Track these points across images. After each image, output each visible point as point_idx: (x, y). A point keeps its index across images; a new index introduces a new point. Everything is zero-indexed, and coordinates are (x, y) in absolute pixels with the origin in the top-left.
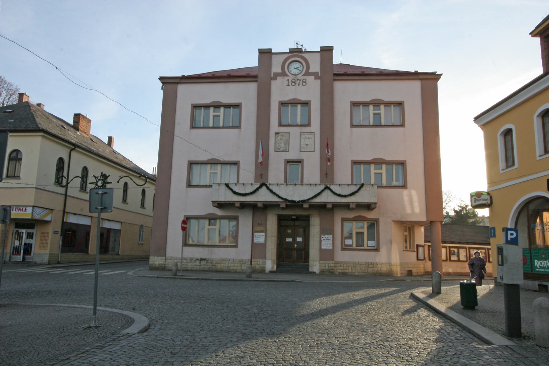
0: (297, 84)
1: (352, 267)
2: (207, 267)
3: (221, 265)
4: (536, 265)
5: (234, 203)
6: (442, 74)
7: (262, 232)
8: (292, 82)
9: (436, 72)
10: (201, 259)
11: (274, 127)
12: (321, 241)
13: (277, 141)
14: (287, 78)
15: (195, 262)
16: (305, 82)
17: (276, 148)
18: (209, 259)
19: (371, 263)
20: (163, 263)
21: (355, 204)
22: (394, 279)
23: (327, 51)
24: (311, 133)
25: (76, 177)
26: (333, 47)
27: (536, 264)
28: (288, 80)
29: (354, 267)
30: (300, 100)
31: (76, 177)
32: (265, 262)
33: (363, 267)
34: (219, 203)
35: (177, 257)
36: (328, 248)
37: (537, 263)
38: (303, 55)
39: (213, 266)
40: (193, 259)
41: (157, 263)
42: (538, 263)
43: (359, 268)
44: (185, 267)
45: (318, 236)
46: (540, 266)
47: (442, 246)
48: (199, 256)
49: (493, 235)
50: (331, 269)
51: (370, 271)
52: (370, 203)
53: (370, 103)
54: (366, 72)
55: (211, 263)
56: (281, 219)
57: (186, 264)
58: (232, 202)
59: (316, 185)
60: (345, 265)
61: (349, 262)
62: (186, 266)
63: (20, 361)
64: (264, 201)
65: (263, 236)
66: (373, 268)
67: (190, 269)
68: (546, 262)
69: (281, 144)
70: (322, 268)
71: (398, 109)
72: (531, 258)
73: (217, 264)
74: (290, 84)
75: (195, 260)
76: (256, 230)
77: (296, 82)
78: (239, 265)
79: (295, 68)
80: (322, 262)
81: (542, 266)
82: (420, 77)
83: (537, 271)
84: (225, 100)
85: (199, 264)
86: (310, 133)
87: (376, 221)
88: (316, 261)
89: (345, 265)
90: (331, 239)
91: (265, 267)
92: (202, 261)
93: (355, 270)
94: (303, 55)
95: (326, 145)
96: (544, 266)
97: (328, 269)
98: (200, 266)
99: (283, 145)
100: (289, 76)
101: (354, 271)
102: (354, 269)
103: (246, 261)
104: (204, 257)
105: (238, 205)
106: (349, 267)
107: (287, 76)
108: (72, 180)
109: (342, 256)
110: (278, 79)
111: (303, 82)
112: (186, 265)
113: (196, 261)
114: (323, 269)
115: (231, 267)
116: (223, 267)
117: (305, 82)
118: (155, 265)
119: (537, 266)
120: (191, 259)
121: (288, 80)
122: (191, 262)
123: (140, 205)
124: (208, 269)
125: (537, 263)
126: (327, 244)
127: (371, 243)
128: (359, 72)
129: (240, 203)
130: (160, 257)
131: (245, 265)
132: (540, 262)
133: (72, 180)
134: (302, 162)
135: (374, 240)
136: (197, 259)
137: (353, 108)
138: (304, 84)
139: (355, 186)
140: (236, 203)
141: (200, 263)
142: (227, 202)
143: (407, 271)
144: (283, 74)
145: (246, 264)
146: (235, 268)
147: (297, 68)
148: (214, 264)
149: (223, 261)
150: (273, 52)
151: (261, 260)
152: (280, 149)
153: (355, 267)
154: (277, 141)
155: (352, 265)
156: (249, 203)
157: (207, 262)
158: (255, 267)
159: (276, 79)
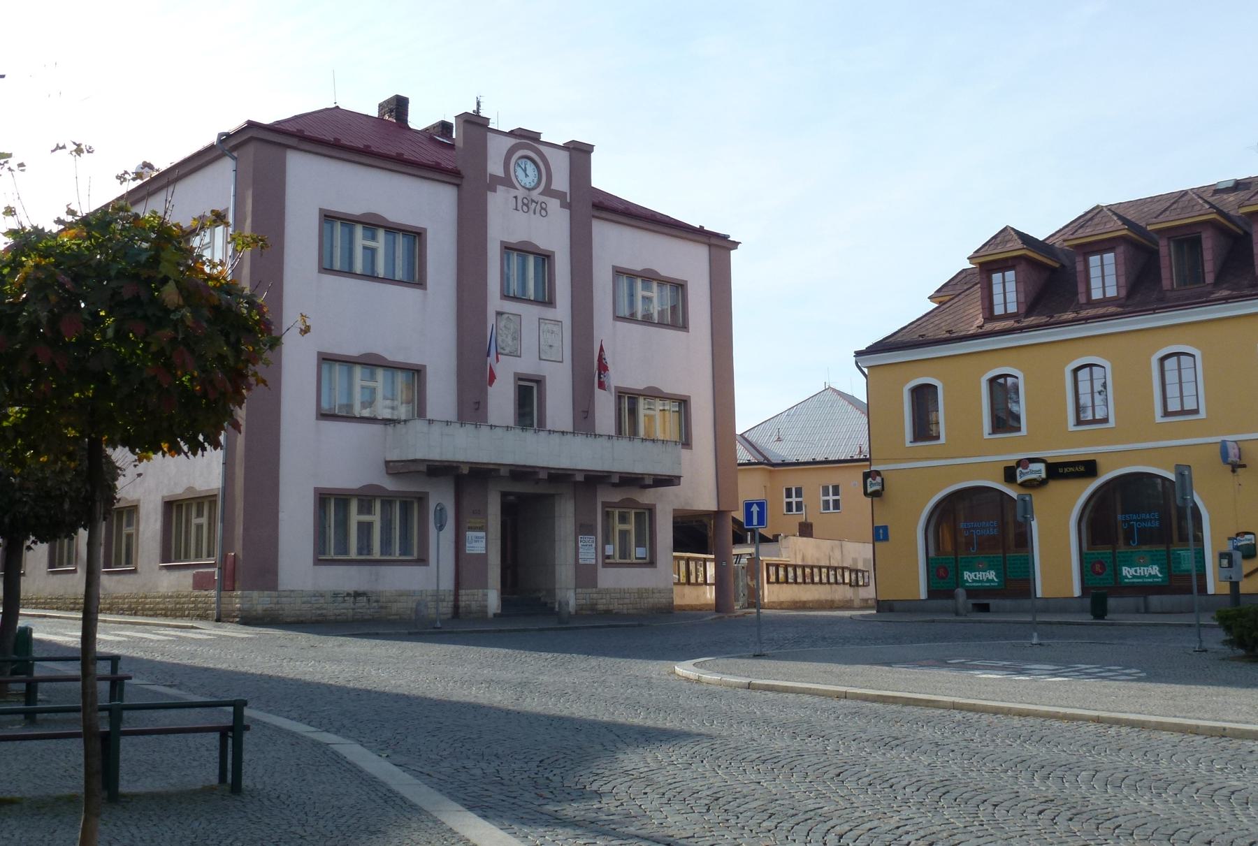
0: (531, 212)
2: (368, 611)
3: (399, 604)
4: (965, 579)
5: (459, 464)
7: (480, 529)
8: (524, 204)
9: (729, 236)
10: (357, 595)
11: (495, 302)
12: (577, 548)
13: (501, 332)
14: (513, 192)
15: (344, 601)
17: (498, 347)
18: (372, 592)
19: (646, 589)
21: (652, 477)
23: (580, 153)
24: (556, 323)
26: (592, 146)
27: (1124, 572)
28: (516, 197)
30: (537, 247)
32: (486, 595)
34: (430, 463)
35: (302, 591)
36: (588, 562)
37: (1126, 571)
38: (542, 148)
39: (381, 607)
40: (339, 594)
41: (260, 608)
42: (969, 576)
44: (322, 614)
45: (572, 538)
46: (973, 580)
47: (674, 556)
48: (351, 586)
49: (881, 537)
52: (673, 476)
53: (639, 274)
54: (607, 203)
55: (377, 601)
56: (335, 499)
58: (455, 464)
59: (563, 433)
60: (608, 596)
61: (615, 589)
62: (324, 611)
63: (520, 798)
64: (472, 463)
65: (482, 538)
67: (333, 618)
68: (984, 573)
69: (507, 337)
72: (957, 567)
73: (390, 604)
74: (519, 208)
75: (344, 597)
76: (469, 525)
77: (529, 205)
79: (527, 175)
80: (579, 590)
81: (977, 579)
82: (714, 241)
83: (1127, 583)
84: (395, 215)
85: (352, 606)
86: (555, 321)
88: (570, 589)
89: (608, 596)
90: (594, 545)
91: (486, 607)
92: (358, 599)
93: (623, 604)
94: (542, 148)
96: (1142, 574)
98: (353, 609)
99: (509, 340)
100: (517, 189)
103: (445, 596)
104: (362, 588)
105: (616, 480)
107: (515, 188)
109: (610, 579)
110: (498, 189)
111: (542, 208)
112: (325, 609)
113: (346, 598)
114: (583, 605)
117: (545, 209)
118: (254, 613)
119: (1126, 576)
120: (336, 595)
121: (516, 197)
122: (334, 602)
124: (371, 617)
125: (1126, 571)
126: (588, 554)
127: (641, 552)
128: (621, 207)
129: (585, 473)
130: (266, 592)
131: (444, 603)
132: (1133, 569)
135: (645, 547)
136: (349, 595)
138: (543, 213)
139: (652, 442)
140: (462, 466)
141: (354, 603)
142: (446, 464)
144: (507, 182)
145: (445, 601)
147: (525, 171)
148: (384, 605)
149: (402, 596)
150: (543, 139)
151: (481, 591)
152: (504, 350)
154: (501, 332)
155: (618, 595)
156: (485, 466)
157: (369, 600)
158: (470, 606)
159: (495, 191)
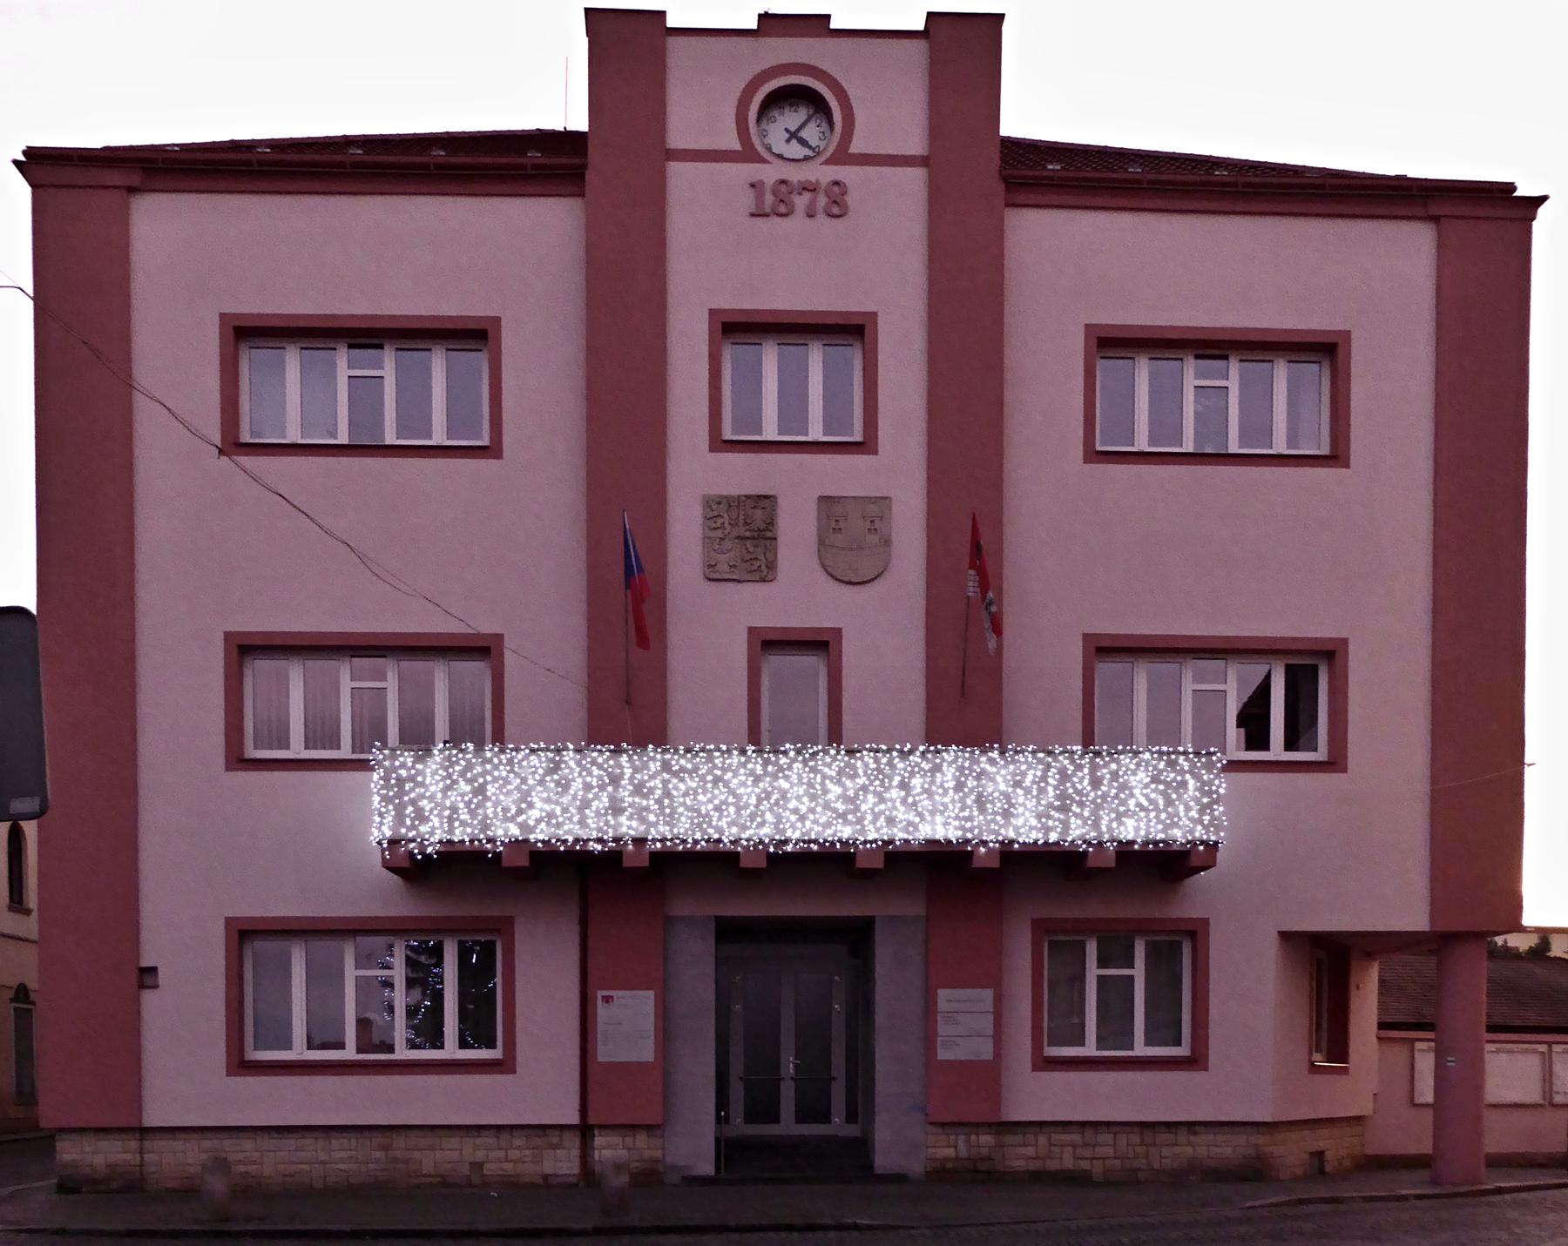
1: (1074, 1146)
6: (1544, 199)
16: (836, 202)
20: (128, 1156)
22: (1295, 1197)
25: (19, 288)
29: (1089, 1145)
31: (19, 288)
33: (1128, 1145)
43: (1110, 1151)
50: (983, 1160)
51: (1161, 1163)
57: (256, 1155)
62: (252, 1168)
66: (1177, 1150)
70: (938, 1156)
71: (1315, 374)
78: (527, 1152)
87: (1192, 935)
95: (966, 548)
97: (969, 1159)
101: (1085, 1165)
102: (1087, 1153)
106: (1062, 1146)
108: (10, 279)
112: (254, 1162)
115: (486, 1166)
116: (449, 1166)
123: (7, 900)
133: (10, 279)
134: (1093, 651)
137: (1102, 366)
143: (1305, 1156)
146: (508, 1166)
153: (1094, 1146)
